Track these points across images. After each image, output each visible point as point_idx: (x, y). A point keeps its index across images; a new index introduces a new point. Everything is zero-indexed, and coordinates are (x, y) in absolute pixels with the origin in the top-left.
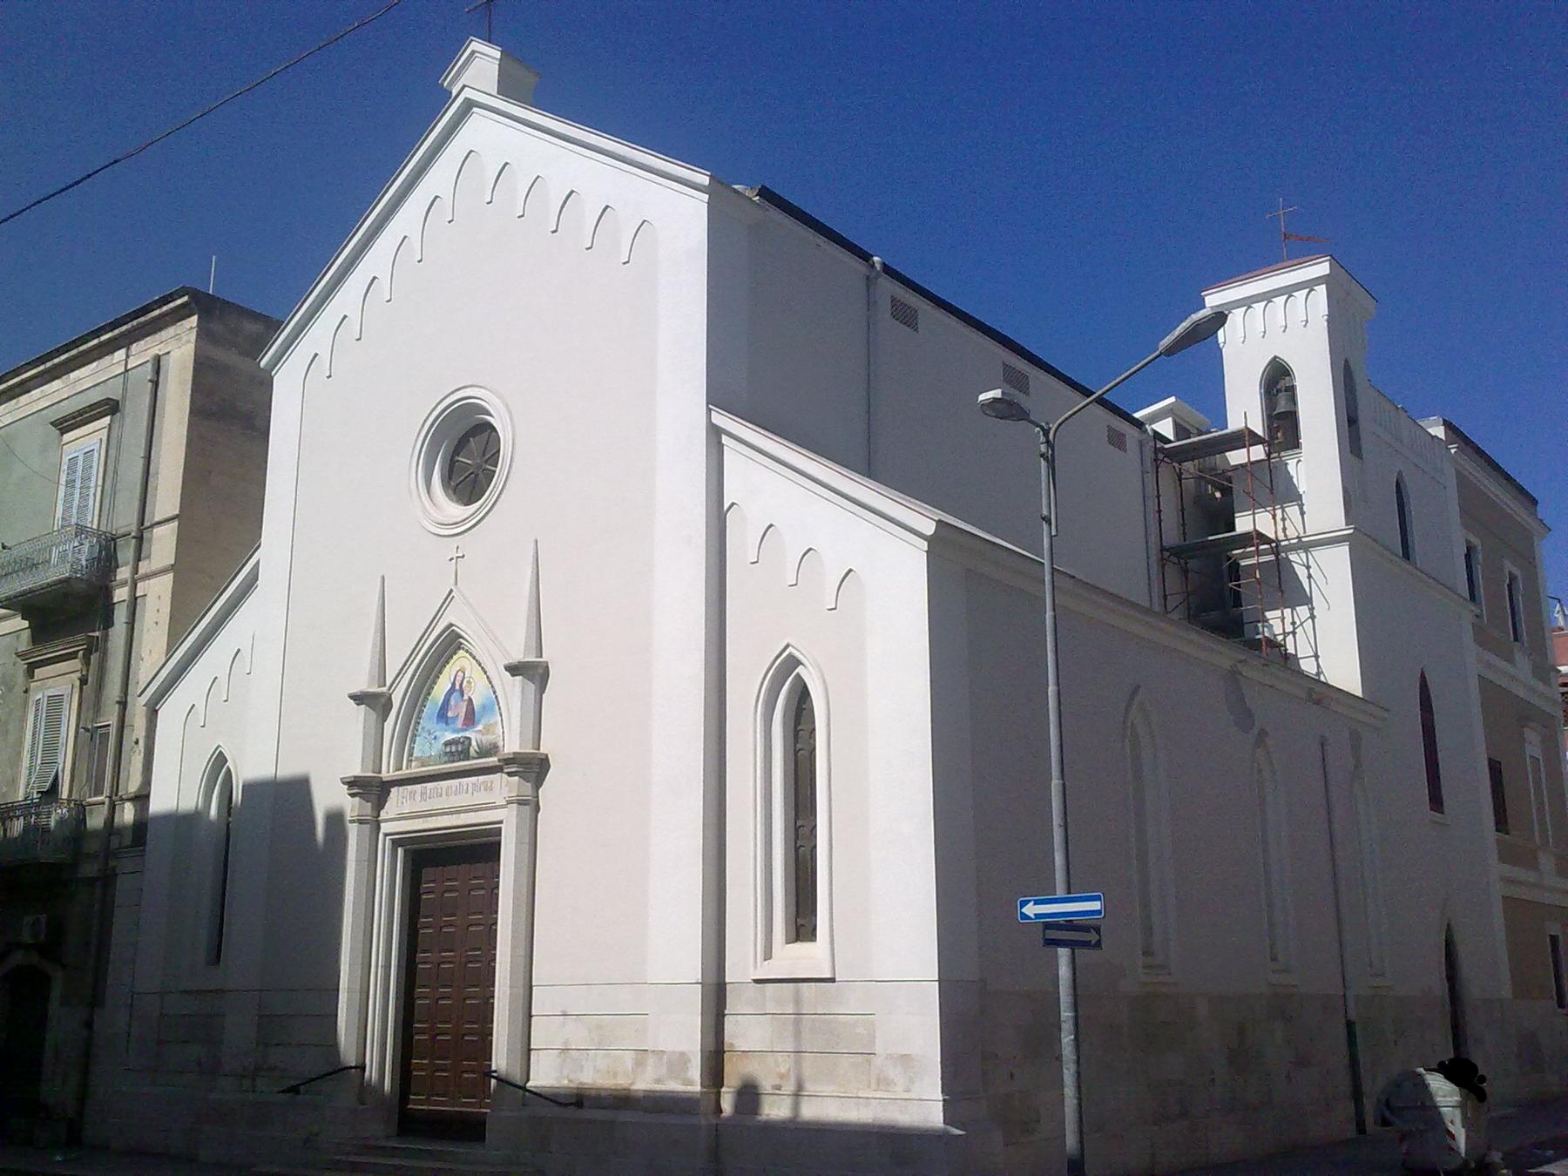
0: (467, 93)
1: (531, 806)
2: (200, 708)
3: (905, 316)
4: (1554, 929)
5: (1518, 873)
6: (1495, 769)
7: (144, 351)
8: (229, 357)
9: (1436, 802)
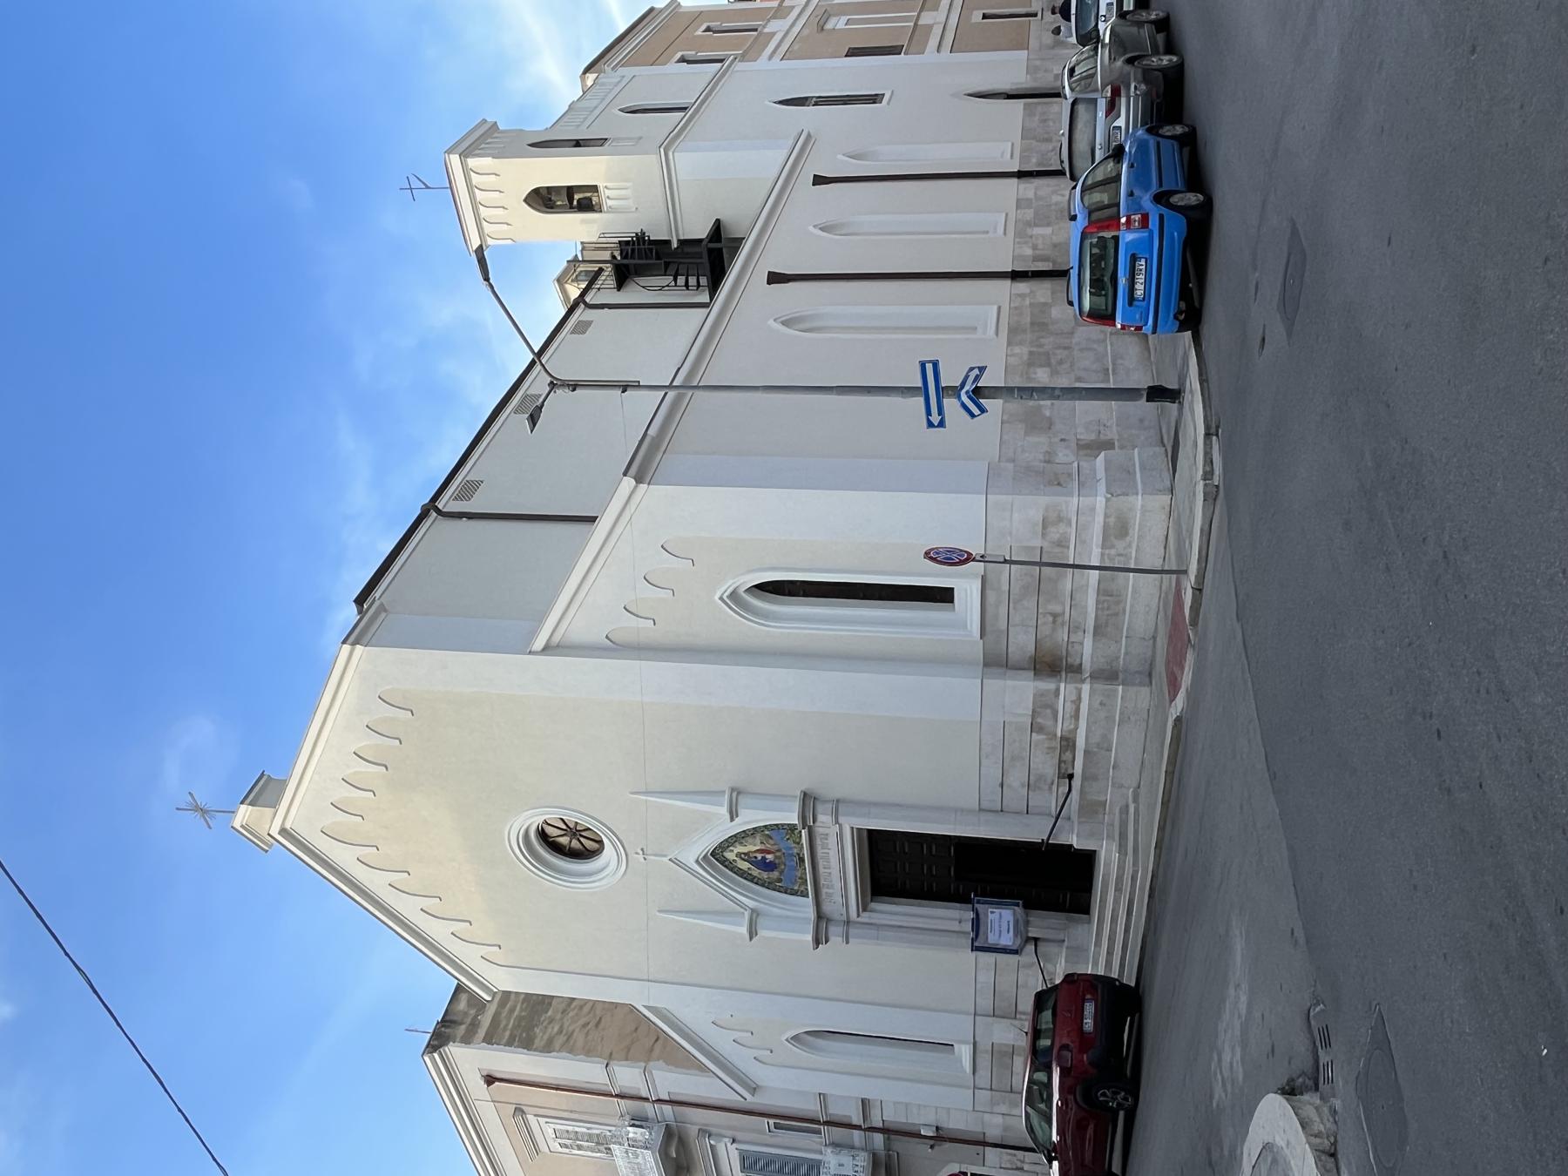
0: (275, 832)
1: (837, 805)
2: (736, 1035)
3: (470, 489)
4: (977, 17)
5: (933, 42)
6: (853, 52)
7: (476, 1086)
8: (486, 1020)
9: (874, 99)
